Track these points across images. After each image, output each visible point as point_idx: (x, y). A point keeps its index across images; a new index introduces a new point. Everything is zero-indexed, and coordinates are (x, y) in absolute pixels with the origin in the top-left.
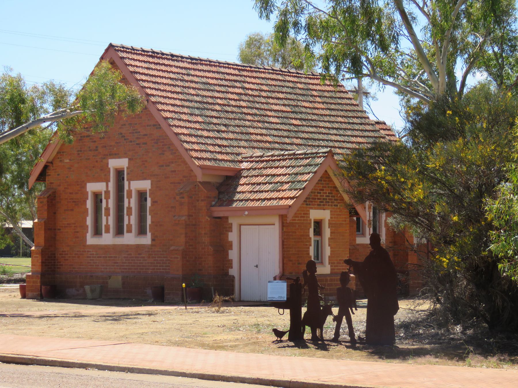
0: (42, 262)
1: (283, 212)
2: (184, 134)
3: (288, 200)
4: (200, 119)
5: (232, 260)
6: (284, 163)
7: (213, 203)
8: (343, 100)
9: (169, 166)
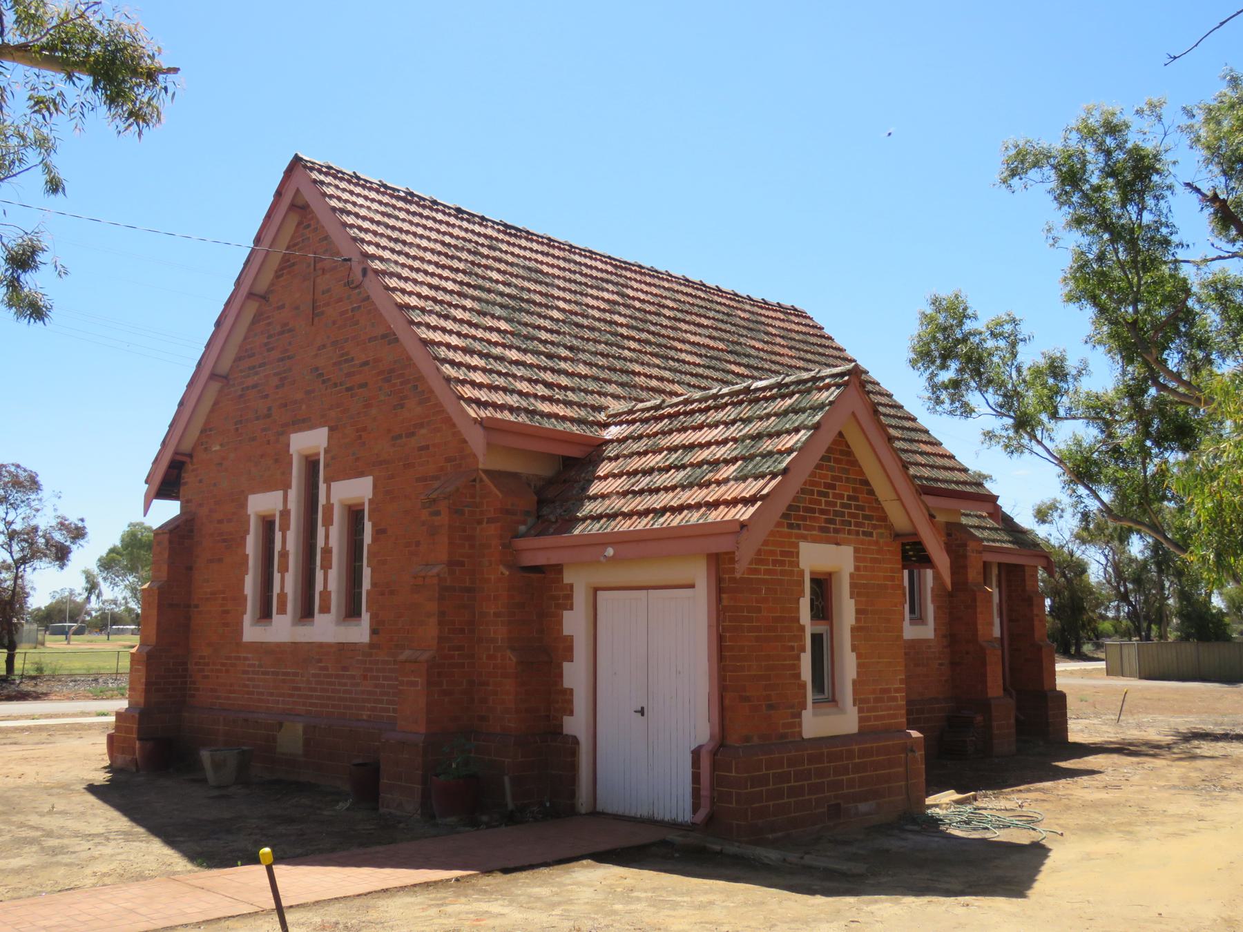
0: (148, 684)
1: (722, 545)
2: (448, 346)
3: (735, 506)
4: (503, 325)
5: (571, 690)
6: (720, 415)
7: (522, 528)
8: (827, 350)
9: (413, 434)
